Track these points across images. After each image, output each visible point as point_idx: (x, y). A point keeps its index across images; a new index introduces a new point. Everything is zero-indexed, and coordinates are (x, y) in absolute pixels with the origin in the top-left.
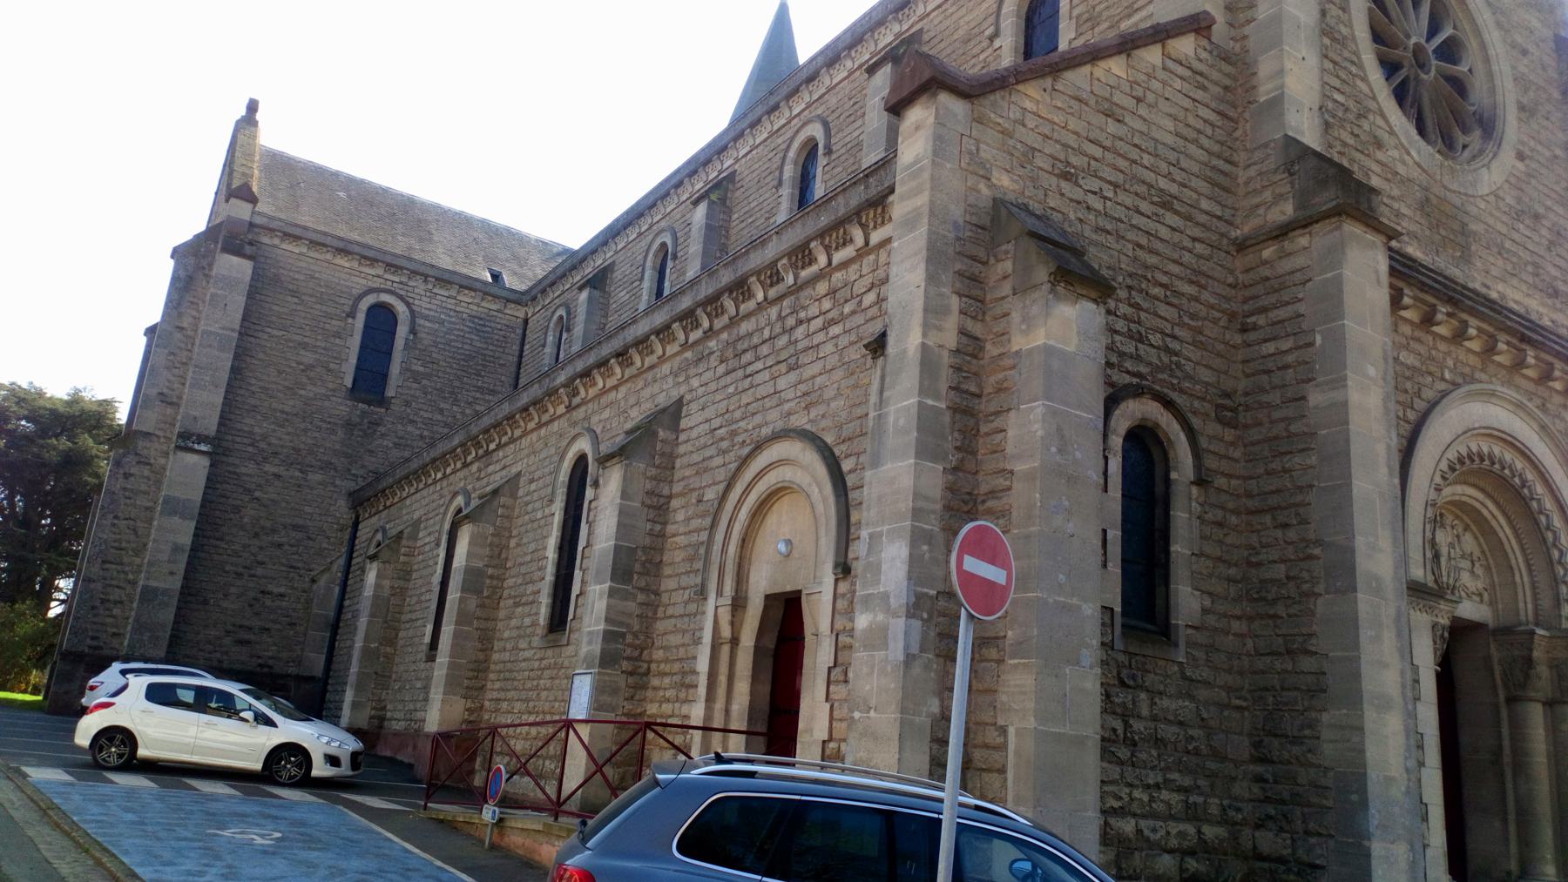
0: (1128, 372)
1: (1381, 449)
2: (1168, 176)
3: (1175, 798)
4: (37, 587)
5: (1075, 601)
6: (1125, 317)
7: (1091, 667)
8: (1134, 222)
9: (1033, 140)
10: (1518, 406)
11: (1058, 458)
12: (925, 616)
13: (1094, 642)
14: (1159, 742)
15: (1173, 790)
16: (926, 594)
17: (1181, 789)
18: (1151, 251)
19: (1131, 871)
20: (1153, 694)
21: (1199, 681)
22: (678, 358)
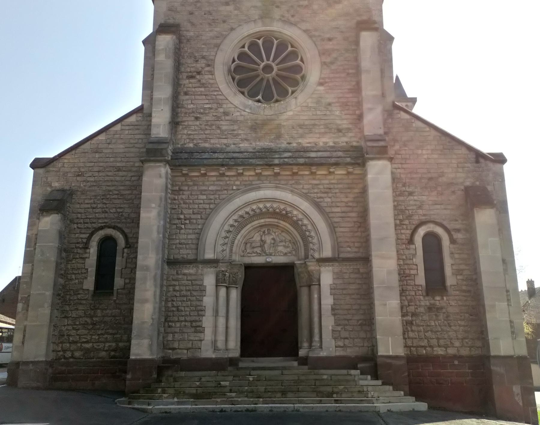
0: (101, 223)
1: (155, 228)
2: (121, 161)
3: (109, 337)
4: (38, 370)
5: (44, 292)
6: (100, 208)
7: (48, 307)
8: (105, 180)
9: (66, 170)
10: (276, 187)
11: (41, 257)
12: (24, 302)
13: (49, 301)
14: (105, 323)
15: (109, 335)
16: (25, 297)
17: (111, 334)
18: (113, 186)
19: (89, 357)
20: (102, 310)
21: (122, 304)
22: (223, 193)
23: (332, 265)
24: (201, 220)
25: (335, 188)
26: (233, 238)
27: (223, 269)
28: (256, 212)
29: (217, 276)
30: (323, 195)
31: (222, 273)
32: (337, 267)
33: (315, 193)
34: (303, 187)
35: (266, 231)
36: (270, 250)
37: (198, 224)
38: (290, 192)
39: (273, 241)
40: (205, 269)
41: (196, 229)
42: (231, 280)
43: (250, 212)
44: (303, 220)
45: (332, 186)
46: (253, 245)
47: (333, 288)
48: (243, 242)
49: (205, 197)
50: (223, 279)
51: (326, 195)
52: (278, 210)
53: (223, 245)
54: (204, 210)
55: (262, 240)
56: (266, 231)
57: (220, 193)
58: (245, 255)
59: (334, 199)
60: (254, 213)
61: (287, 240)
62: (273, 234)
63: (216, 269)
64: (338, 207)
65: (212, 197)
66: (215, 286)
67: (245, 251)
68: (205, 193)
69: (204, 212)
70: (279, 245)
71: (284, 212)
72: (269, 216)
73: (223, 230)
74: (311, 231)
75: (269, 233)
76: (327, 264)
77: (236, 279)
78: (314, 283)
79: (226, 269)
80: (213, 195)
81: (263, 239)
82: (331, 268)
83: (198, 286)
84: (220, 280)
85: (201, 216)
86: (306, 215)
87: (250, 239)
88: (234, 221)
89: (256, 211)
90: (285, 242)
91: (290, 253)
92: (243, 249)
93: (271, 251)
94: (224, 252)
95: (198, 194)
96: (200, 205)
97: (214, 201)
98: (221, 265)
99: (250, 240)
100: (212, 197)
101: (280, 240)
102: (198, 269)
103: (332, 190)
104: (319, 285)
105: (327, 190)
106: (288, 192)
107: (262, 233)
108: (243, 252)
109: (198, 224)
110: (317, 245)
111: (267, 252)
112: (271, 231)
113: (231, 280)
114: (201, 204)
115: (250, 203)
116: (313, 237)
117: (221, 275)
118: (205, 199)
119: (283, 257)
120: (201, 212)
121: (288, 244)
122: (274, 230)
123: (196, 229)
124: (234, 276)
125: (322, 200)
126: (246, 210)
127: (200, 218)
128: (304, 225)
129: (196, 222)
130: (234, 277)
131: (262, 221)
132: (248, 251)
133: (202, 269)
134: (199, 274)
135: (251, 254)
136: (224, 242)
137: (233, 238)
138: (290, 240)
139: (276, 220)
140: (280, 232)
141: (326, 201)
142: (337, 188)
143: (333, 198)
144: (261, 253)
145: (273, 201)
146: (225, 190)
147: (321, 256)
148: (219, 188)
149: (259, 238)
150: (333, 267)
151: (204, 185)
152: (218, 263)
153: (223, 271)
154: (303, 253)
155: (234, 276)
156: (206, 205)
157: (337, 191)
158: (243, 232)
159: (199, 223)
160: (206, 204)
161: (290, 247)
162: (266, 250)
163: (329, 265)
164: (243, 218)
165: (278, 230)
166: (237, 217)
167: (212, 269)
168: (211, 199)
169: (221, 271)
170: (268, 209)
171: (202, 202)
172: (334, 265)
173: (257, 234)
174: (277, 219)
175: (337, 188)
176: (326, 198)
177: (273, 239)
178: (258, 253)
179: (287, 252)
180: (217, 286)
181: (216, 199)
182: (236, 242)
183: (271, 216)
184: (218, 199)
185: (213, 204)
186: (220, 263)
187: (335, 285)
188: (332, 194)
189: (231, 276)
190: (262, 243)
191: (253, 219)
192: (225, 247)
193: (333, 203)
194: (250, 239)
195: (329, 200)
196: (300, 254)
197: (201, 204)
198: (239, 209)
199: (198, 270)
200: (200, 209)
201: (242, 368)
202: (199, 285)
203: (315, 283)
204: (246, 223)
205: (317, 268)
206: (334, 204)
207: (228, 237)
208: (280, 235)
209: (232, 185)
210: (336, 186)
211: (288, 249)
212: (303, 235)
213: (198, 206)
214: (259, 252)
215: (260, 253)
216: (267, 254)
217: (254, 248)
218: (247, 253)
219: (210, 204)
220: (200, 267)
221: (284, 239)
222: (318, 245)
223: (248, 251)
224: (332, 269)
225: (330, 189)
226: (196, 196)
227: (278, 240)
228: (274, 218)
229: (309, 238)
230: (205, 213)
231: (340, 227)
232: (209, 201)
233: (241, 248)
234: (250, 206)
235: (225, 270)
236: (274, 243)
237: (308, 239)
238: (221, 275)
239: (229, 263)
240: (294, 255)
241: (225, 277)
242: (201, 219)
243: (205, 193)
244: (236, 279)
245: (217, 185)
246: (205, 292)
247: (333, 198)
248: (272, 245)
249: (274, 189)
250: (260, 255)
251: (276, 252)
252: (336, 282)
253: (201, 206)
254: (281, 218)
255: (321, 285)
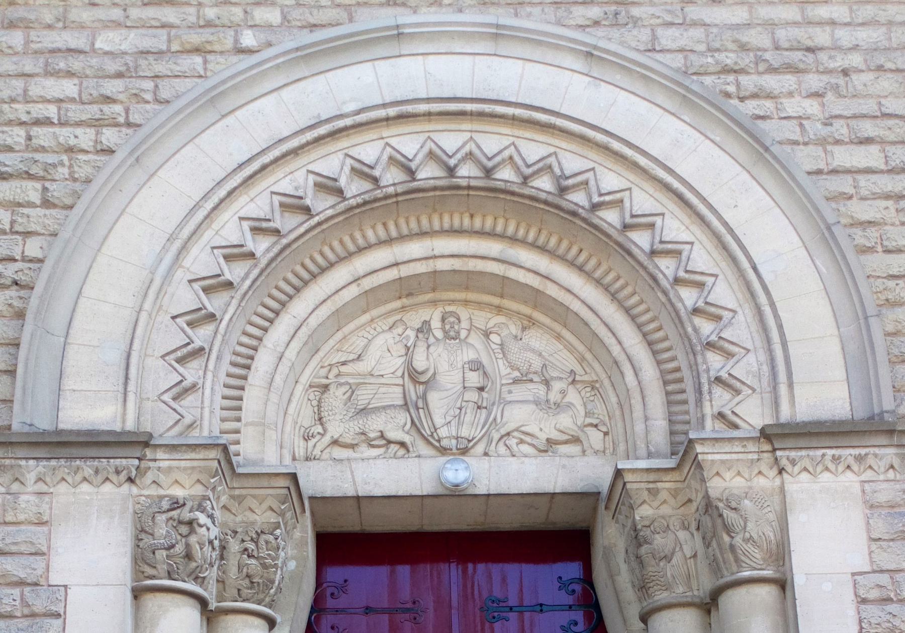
23: (860, 459)
24: (40, 211)
25: (838, 48)
26: (245, 340)
27: (179, 493)
28: (375, 180)
29: (141, 531)
30: (771, 82)
31: (174, 513)
32: (891, 474)
33: (727, 70)
34: (654, 37)
35: (436, 324)
36: (460, 424)
37: (27, 234)
38: (578, 64)
39: (474, 379)
40: (63, 488)
41: (13, 260)
42: (233, 572)
43: (343, 182)
44: (658, 221)
45: (822, 37)
46: (363, 397)
47: (874, 594)
48: (305, 379)
49: (69, 87)
50: (179, 549)
51: (788, 81)
52: (506, 174)
53: (179, 361)
54: (65, 158)
55: (413, 375)
56: (436, 324)
57: (161, 68)
58: (317, 452)
59: (837, 106)
60: (367, 185)
61: (555, 374)
62: (475, 340)
63: (135, 490)
64: (868, 141)
65: (112, 87)
66: (129, 595)
67: (320, 429)
68: (76, 64)
69: (65, 171)
70: (509, 398)
71: (544, 183)
72: (456, 223)
73: (181, 276)
74: (710, 280)
75: (451, 336)
76: (830, 452)
77: (265, 566)
78: (747, 574)
79: (199, 490)
80: (119, 75)
81: (420, 363)
82: (850, 480)
83: (16, 592)
84: (161, 554)
85: (45, 189)
86: (676, 184)
87: (344, 363)
88: (246, 225)
89: (376, 173)
90: (547, 383)
91: (576, 440)
92: (307, 418)
93: (465, 432)
94: (190, 400)
95: (28, 68)
96: (36, 131)
97: (127, 111)
98: (164, 464)
99: (343, 369)
100: (112, 87)
101: (516, 374)
102: (15, 487)
103: (823, 56)
104: (783, 584)
105: (796, 56)
106: (569, 61)
107: (411, 334)
108: (306, 439)
109: (27, 234)
110: (751, 358)
111: (443, 432)
112: (465, 324)
113: (233, 572)
114: (46, 122)
115: (341, 123)
116: (727, 315)
117: (162, 528)
118: (73, 100)
119: (533, 460)
120: (47, 167)
121: (563, 393)
122: (482, 319)
123: (13, 260)
124: (251, 546)
125: (769, 104)
126: (317, 167)
127: (35, 197)
128: (668, 253)
129: (13, 222)
130: (250, 556)
131: (415, 248)
132: (335, 429)
133: (42, 487)
134: (22, 517)
135: (352, 446)
136: (181, 340)
137: (245, 340)
138: (572, 372)
139: (494, 248)
140: (514, 329)
141: (791, 112)
142: (856, 48)
143: (830, 96)
144: (407, 439)
145: (481, 115)
146: (197, 50)
147: (785, 414)
148: (158, 41)
149: (395, 363)
150: (869, 475)
151: (65, 23)
152: (149, 453)
153: (177, 504)
154: (660, 425)
155: (251, 546)
156: (79, 131)
157: (856, 60)
158: (300, 307)
159: (33, 227)
160: (79, 124)
161: (570, 405)
162: (438, 421)
163: (836, 459)
164: (300, 218)
165: (501, 319)
166: (267, 208)
167: (108, 488)
168: (108, 100)
169: (165, 505)
170: (452, 162)
171: (52, 111)
172: (871, 461)
173: (388, 339)
174: (502, 237)
175: (856, 48)
176: (790, 94)
177: (477, 366)
178: (390, 442)
179: (555, 435)
180: (138, 593)
181: (137, 97)
182: (263, 361)
183: (467, 221)
184: (148, 97)
185: (117, 125)
186: (160, 455)
187: (884, 579)
188: (825, 78)
189: (234, 546)
190: (410, 386)
191: (358, 235)
192: (191, 372)
193: (838, 124)
194: (344, 363)
195: (812, 107)
196: (639, 427)
197: (46, 122)
198: (276, 153)
199: (16, 495)
200: (43, 149)
201: (240, 474)
202: (21, 583)
203: (755, 573)
204: (319, 259)
205: (767, 482)
206: (840, 129)
207: (211, 317)
208: (513, 348)
209: (236, 27)
210: (845, 36)
211: (565, 421)
212: (652, 320)
213: (29, 138)
214: (394, 434)
215: (402, 444)
216: (445, 443)
217: (364, 411)
218: (327, 439)
219: (97, 123)
220: (31, 477)
221: (537, 364)
222: (763, 357)
223: (335, 429)
224: (857, 489)
225: (809, 50)
226: (19, 84)
227: (504, 370)
228: (481, 233)
229: (698, 321)
230: (71, 174)
231: (888, 251)
232: (95, 108)
233: (291, 410)
234: (343, 143)
235: (193, 498)
236: (481, 389)
237: (696, 330)
238: (162, 528)
239: (213, 454)
240: (596, 452)
241: (193, 539)
242: (47, 203)
243: (76, 64)
244: (265, 566)
245: (143, 25)
246: (59, 622)
247: (830, 96)
248: (473, 396)
249: (479, 47)
250: (402, 452)
251: (496, 436)
252: (887, 560)
253: (43, 136)
254: (521, 233)
255: (799, 580)
